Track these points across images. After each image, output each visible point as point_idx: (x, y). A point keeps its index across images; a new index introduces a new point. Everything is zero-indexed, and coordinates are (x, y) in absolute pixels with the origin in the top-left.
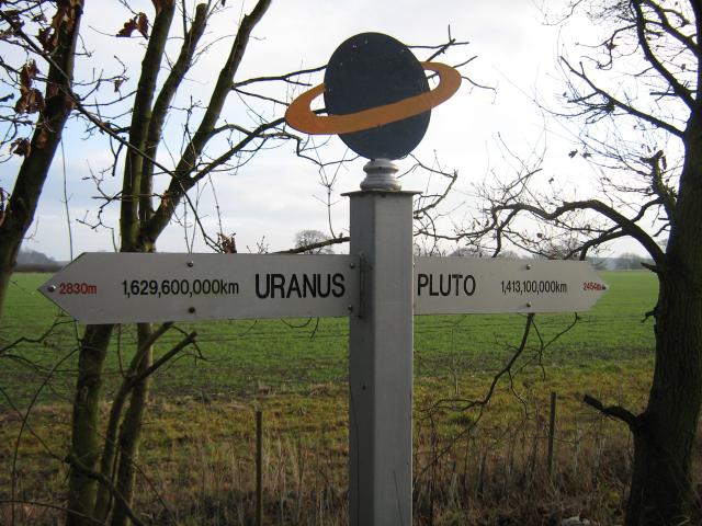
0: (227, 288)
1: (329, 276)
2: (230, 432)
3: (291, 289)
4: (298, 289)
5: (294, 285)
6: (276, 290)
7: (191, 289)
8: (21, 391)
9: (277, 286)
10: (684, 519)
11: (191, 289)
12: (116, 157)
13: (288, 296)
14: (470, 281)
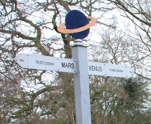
0: (52, 64)
1: (62, 63)
2: (106, 84)
3: (66, 66)
4: (67, 66)
5: (67, 65)
6: (66, 67)
7: (45, 64)
8: (18, 68)
9: (70, 66)
10: (12, 88)
11: (45, 64)
12: (128, 17)
13: (66, 67)
14: (44, 64)
